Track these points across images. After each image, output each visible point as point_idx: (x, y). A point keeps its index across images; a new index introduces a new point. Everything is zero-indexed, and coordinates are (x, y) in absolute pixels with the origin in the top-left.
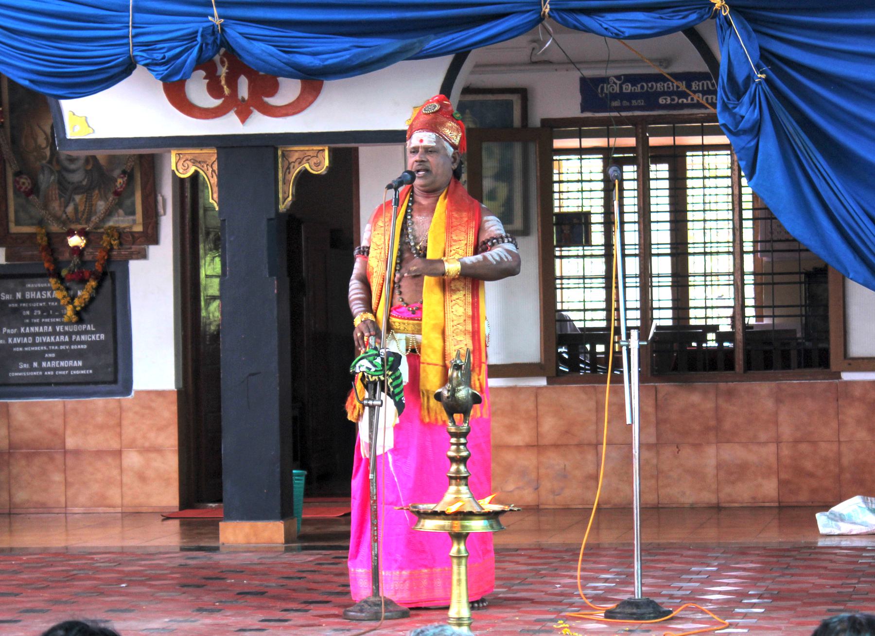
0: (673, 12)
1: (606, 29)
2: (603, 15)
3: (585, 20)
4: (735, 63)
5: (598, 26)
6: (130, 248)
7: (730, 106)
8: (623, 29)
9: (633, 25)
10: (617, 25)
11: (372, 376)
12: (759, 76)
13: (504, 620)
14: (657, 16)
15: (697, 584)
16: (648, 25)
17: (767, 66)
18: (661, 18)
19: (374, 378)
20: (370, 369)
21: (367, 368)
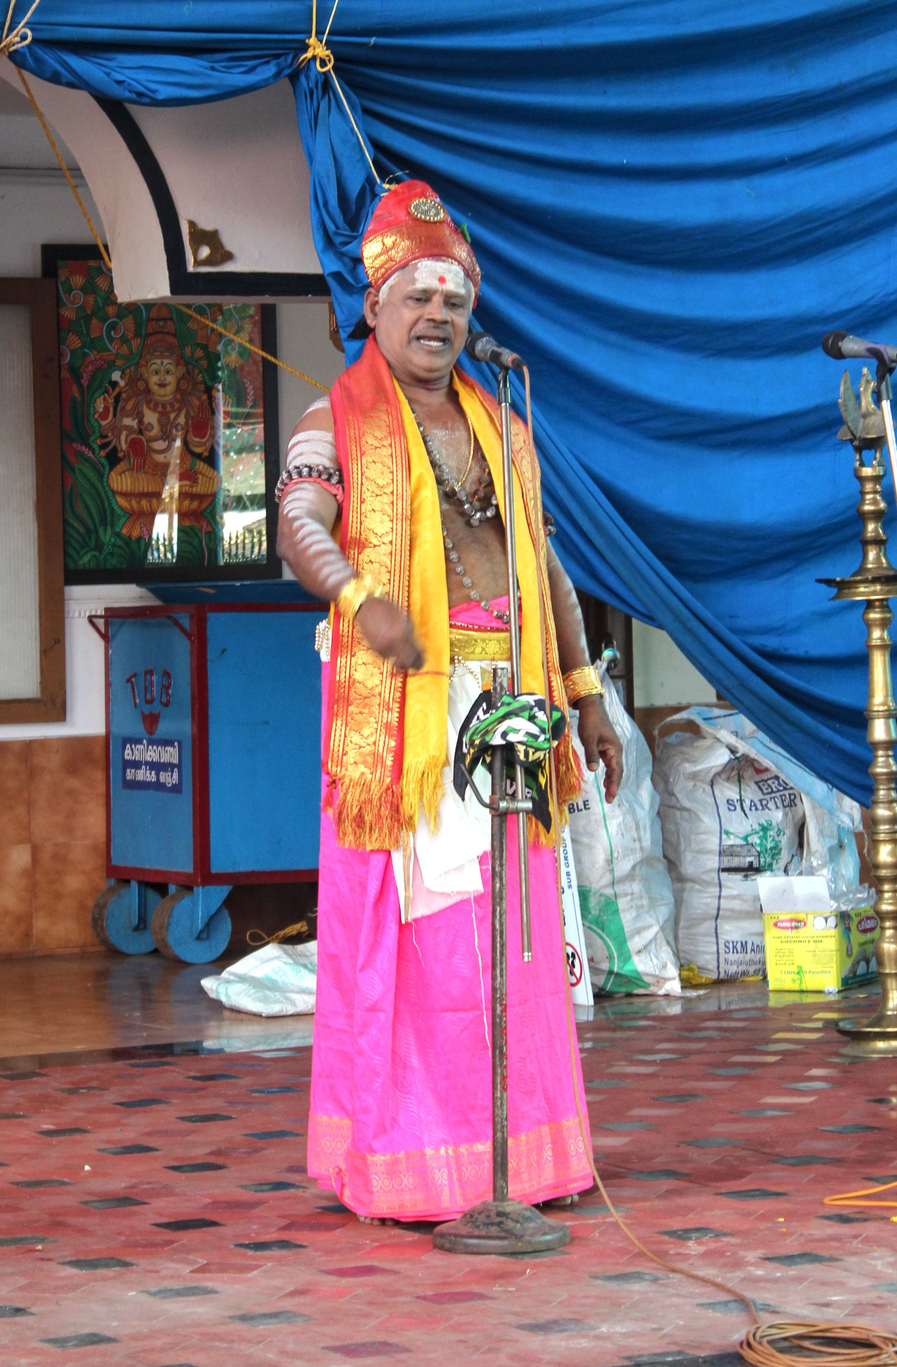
0: (231, 59)
1: (119, 82)
2: (110, 56)
3: (76, 62)
4: (344, 161)
5: (102, 75)
6: (506, 401)
7: (338, 240)
8: (153, 86)
9: (172, 79)
10: (142, 76)
11: (537, 750)
12: (386, 186)
13: (23, 1175)
14: (208, 65)
15: (816, 1016)
16: (196, 81)
17: (402, 170)
18: (213, 69)
19: (537, 755)
20: (536, 737)
21: (528, 734)
